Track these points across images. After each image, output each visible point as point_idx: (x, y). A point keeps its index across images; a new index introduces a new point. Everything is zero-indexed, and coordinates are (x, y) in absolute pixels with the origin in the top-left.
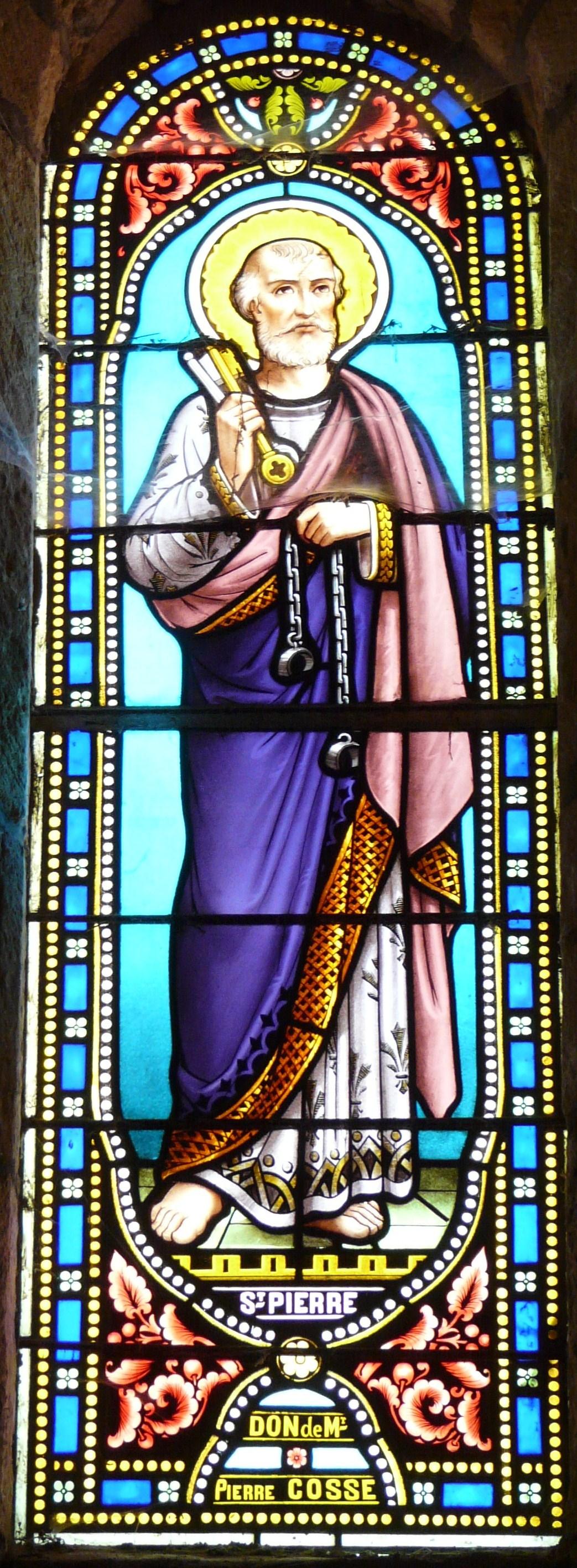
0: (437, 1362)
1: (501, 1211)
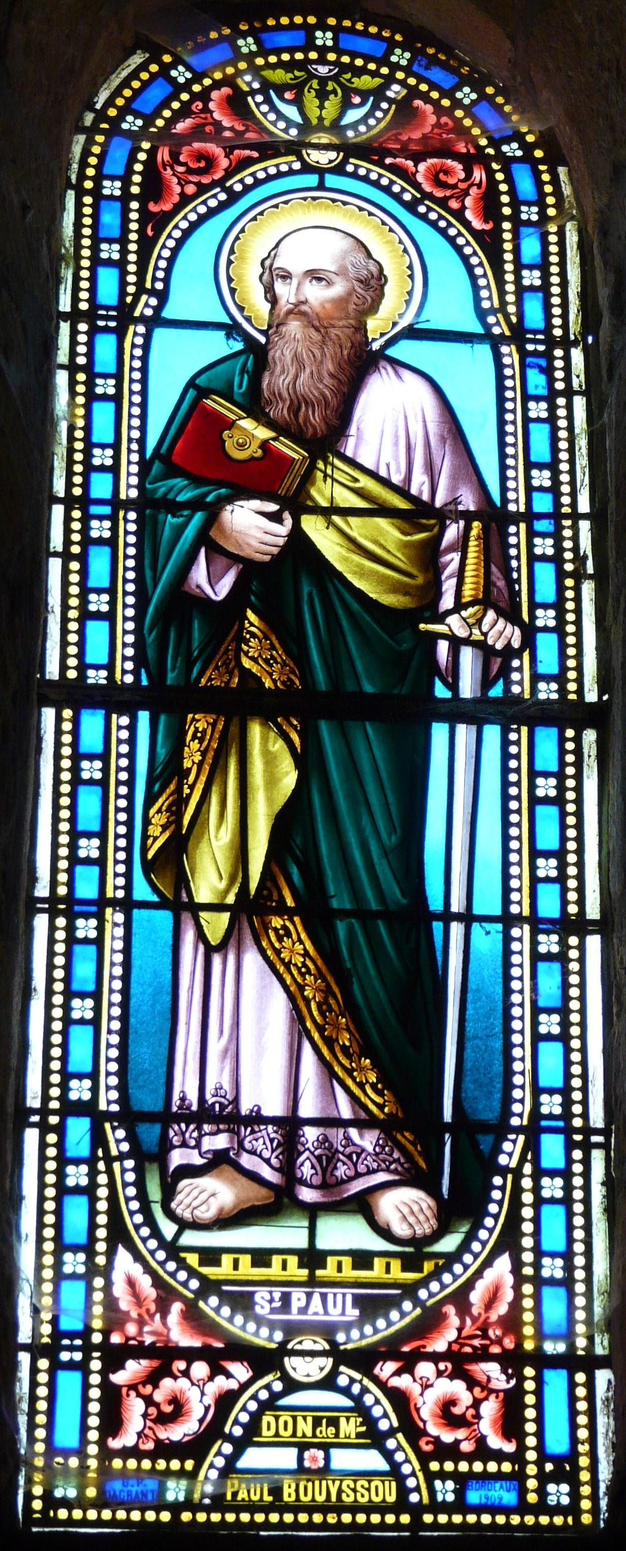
0: (458, 1363)
1: (527, 1212)
